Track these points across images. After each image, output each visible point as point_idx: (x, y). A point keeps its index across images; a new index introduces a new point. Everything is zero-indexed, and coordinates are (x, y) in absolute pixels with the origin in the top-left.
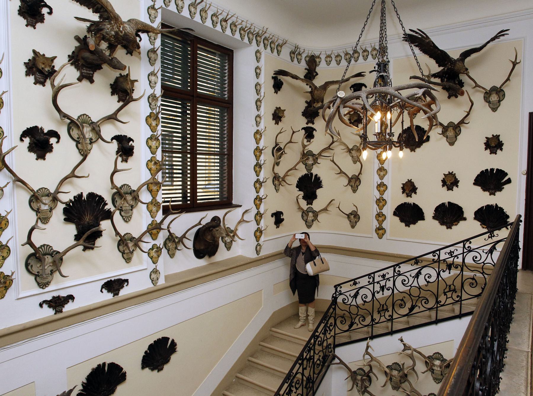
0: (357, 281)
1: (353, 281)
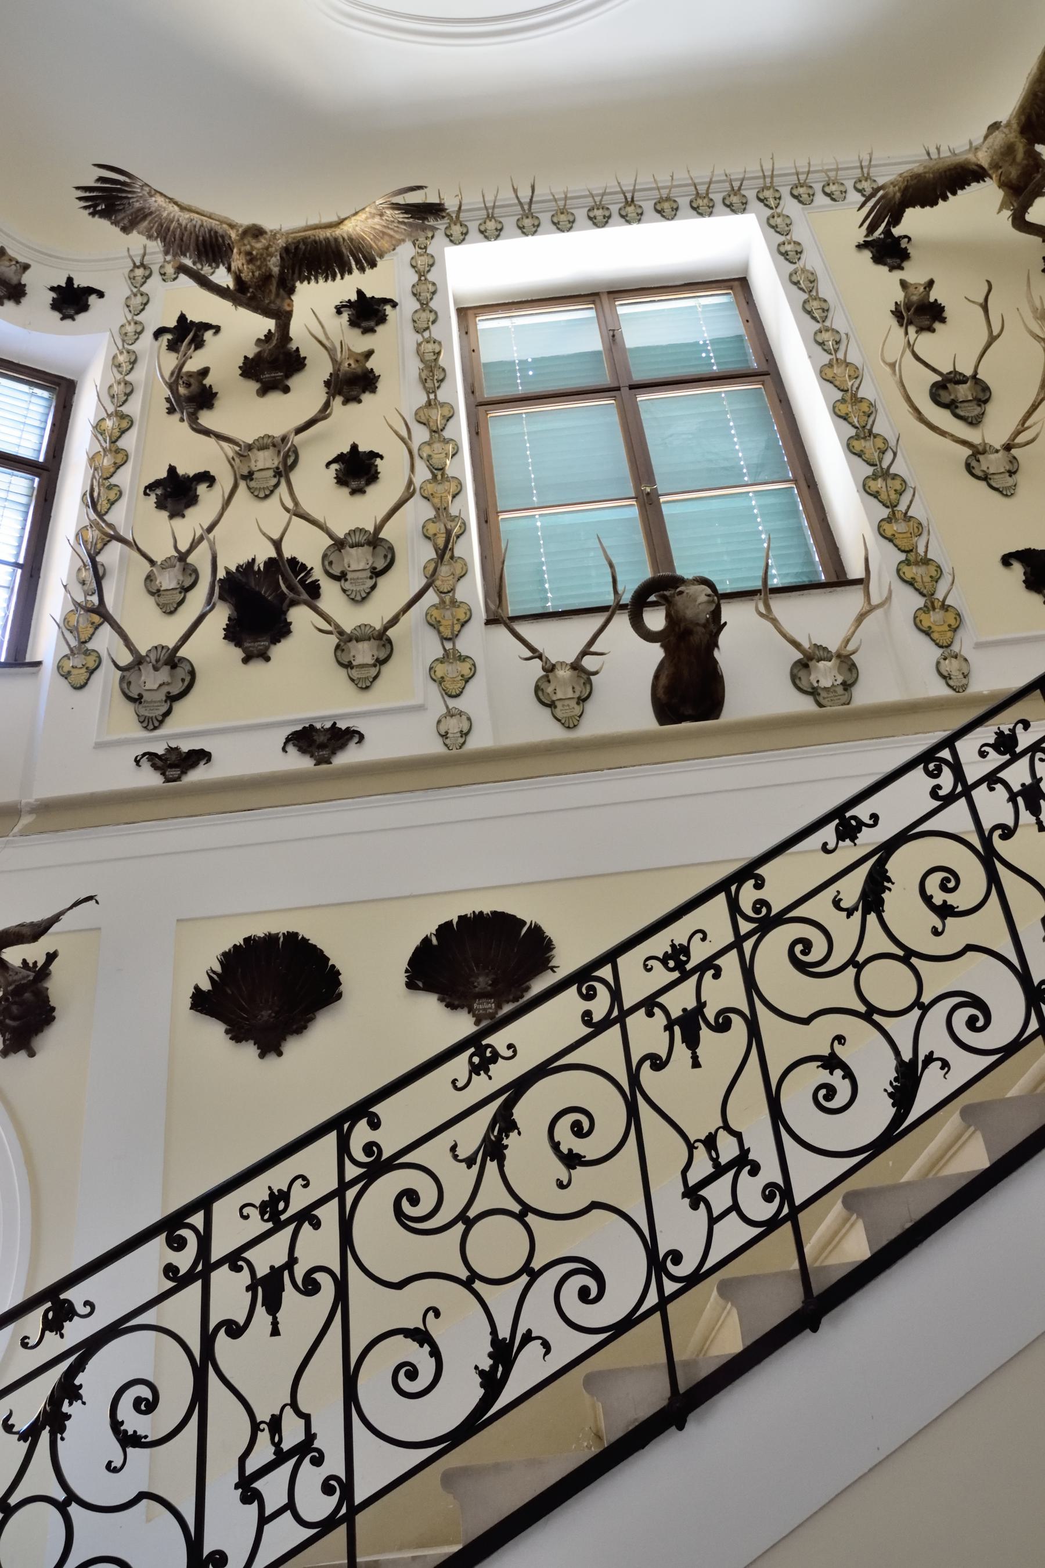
0: (75, 1295)
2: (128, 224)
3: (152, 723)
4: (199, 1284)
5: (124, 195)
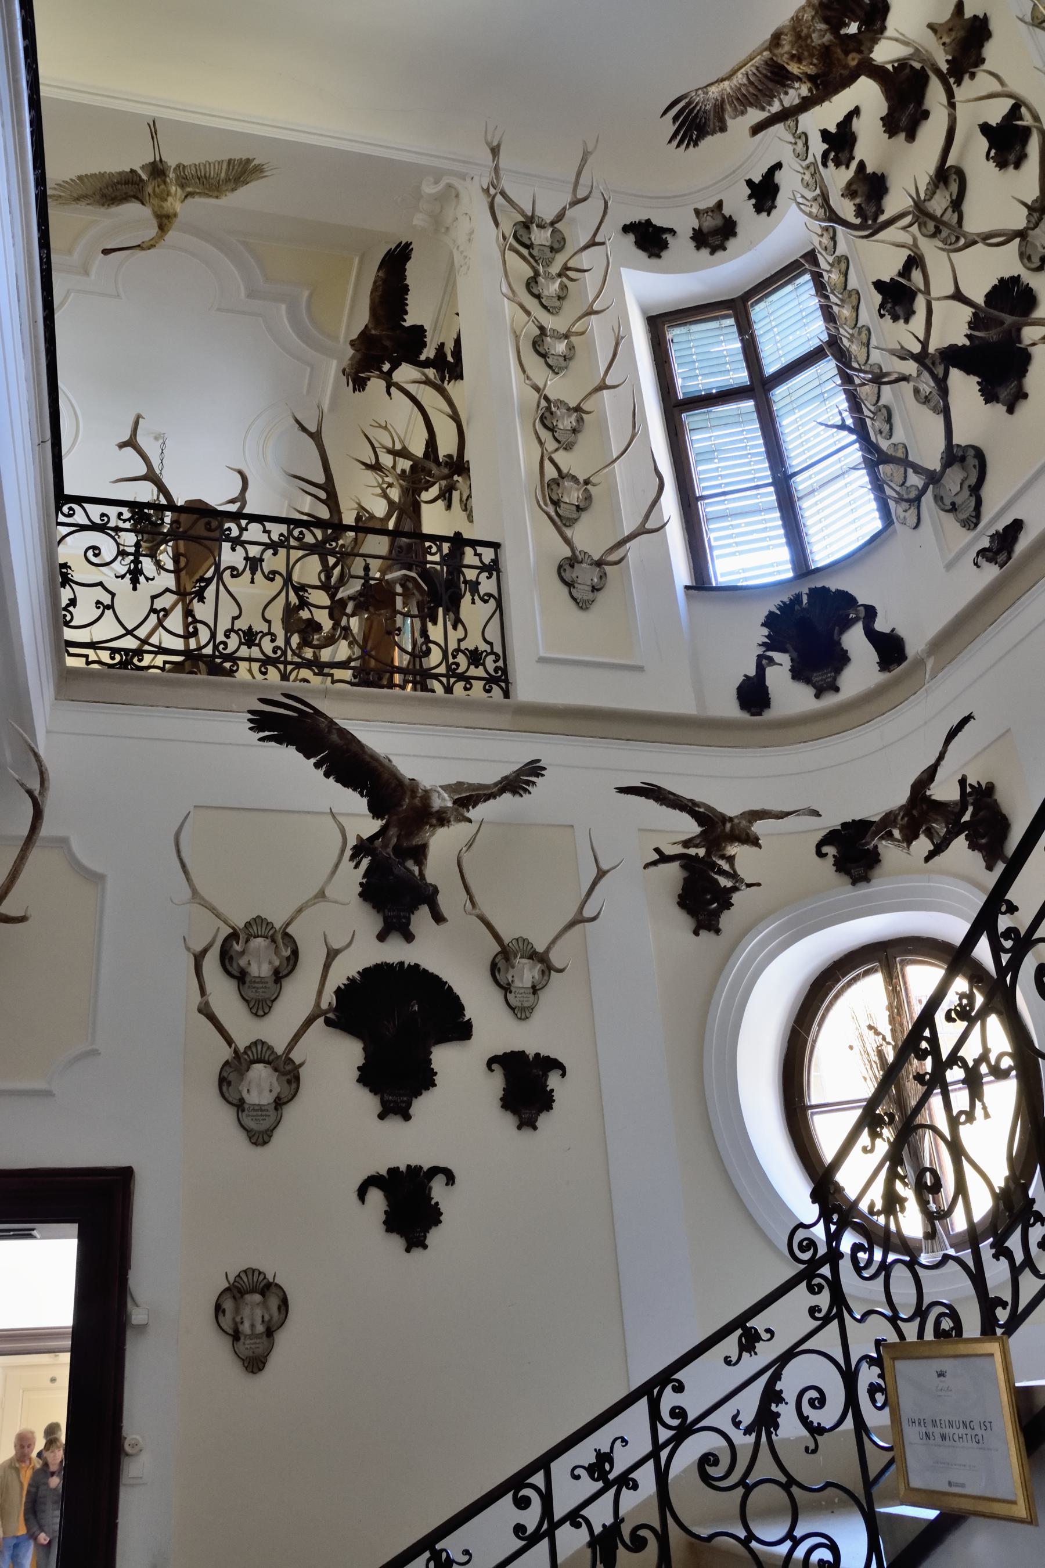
0: (757, 1323)
1: (739, 1332)
2: (720, 124)
3: (972, 522)
4: (546, 1541)
5: (695, 111)
